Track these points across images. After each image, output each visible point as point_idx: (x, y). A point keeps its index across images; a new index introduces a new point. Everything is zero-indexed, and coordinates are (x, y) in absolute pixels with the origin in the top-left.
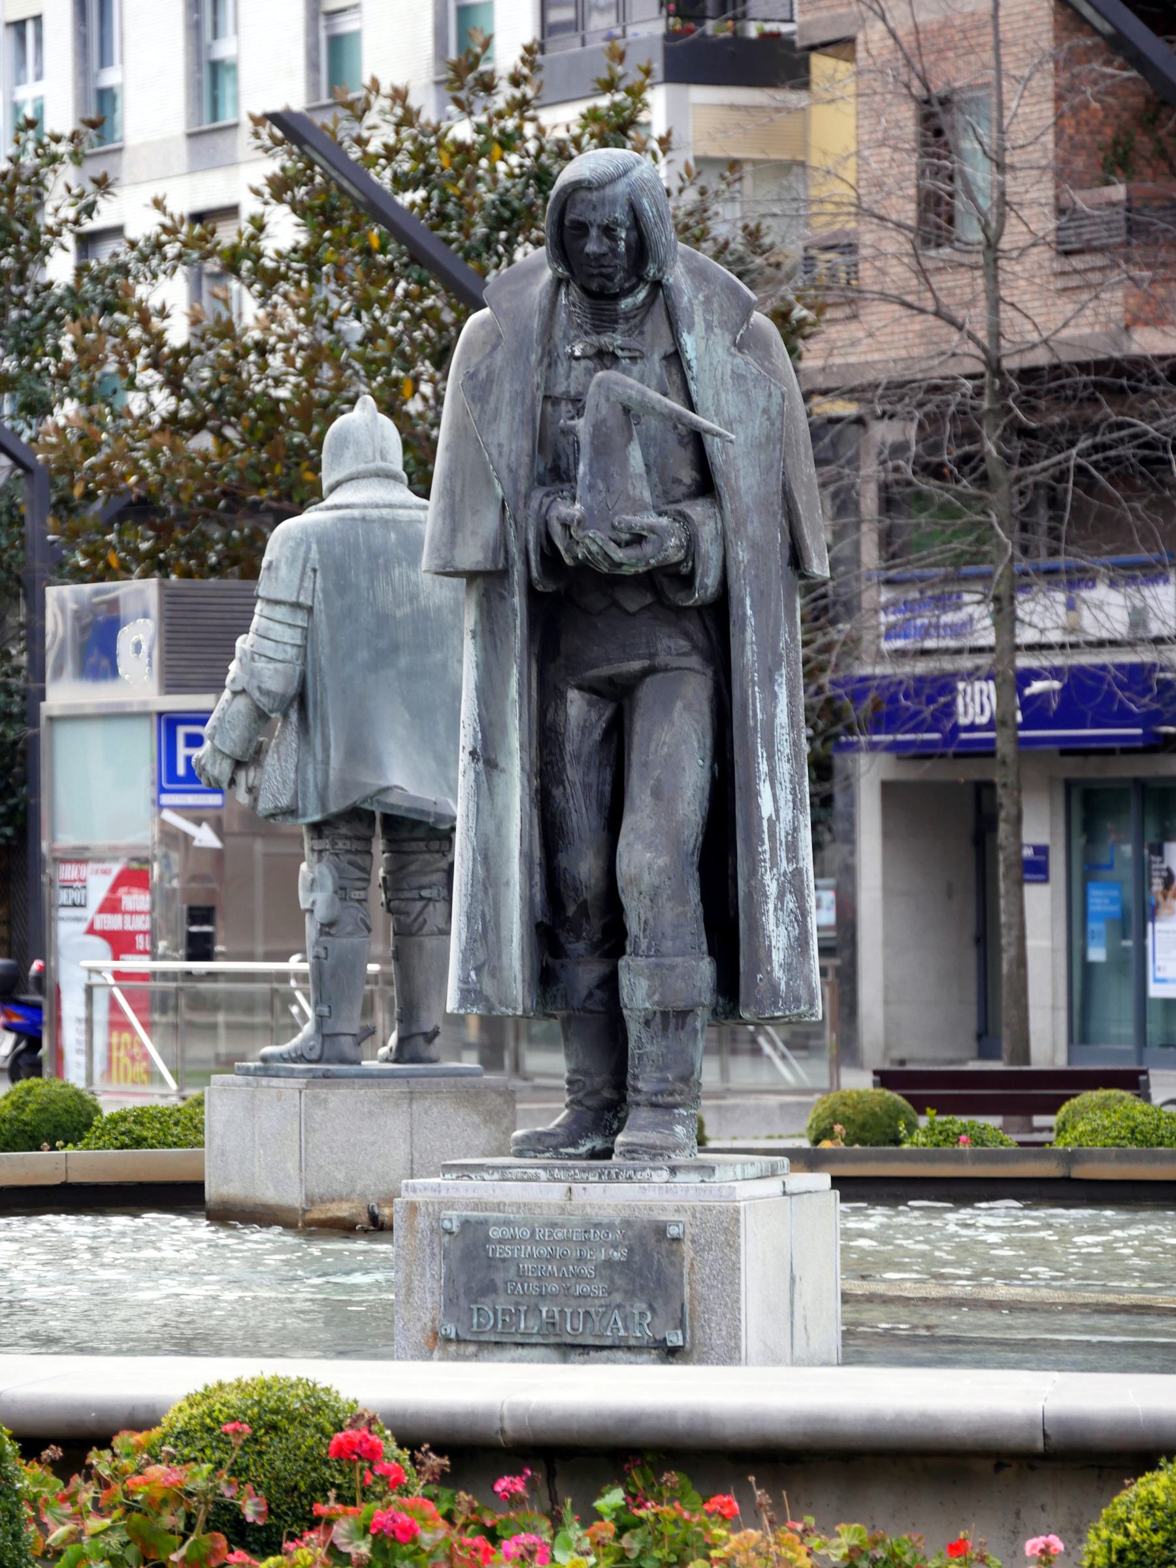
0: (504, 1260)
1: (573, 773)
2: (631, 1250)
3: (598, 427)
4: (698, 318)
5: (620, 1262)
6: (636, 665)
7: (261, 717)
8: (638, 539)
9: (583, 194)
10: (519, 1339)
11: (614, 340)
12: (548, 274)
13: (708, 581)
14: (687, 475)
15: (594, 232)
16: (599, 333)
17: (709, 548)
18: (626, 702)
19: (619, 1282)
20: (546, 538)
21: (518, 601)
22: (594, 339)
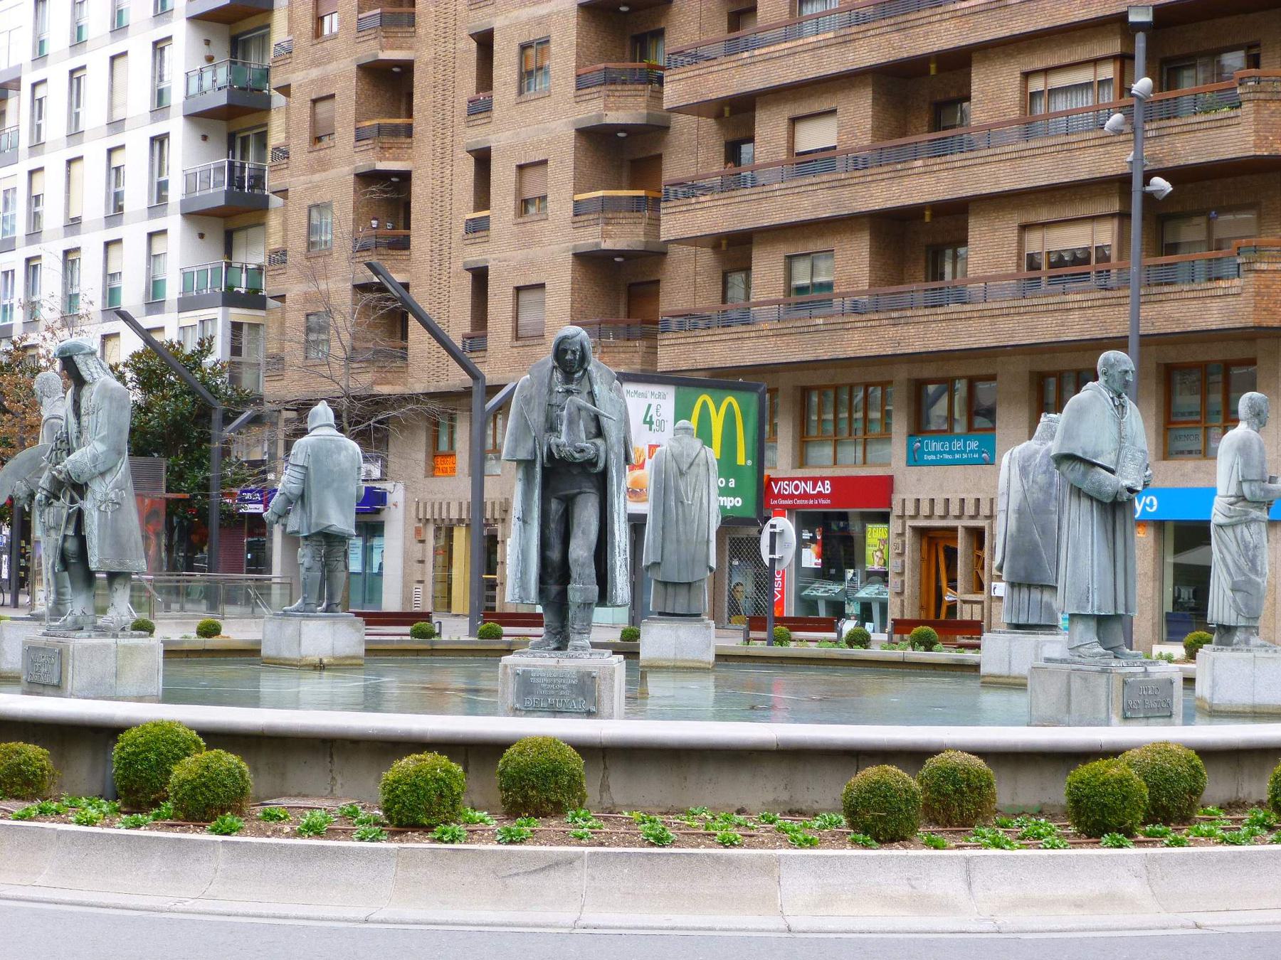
1: (553, 526)
3: (570, 414)
7: (289, 502)
8: (582, 451)
11: (573, 387)
12: (550, 364)
13: (601, 465)
14: (593, 430)
17: (602, 455)
20: (550, 449)
21: (538, 469)
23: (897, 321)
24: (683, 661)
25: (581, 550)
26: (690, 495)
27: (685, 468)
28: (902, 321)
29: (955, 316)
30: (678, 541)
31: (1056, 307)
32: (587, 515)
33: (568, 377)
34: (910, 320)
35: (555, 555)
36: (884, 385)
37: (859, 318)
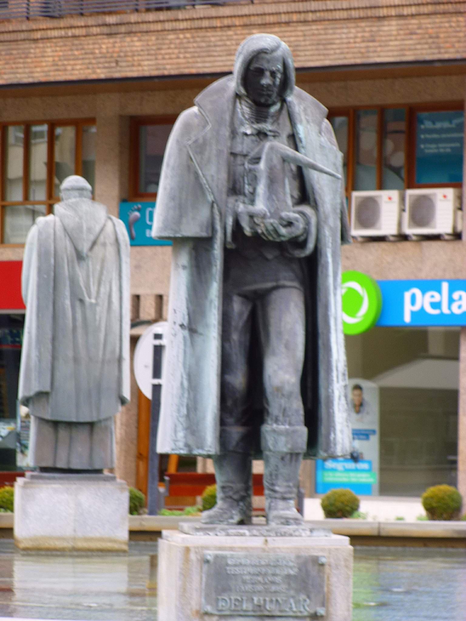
0: (234, 575)
2: (300, 569)
3: (271, 169)
4: (303, 117)
5: (295, 576)
6: (269, 285)
8: (290, 224)
9: (263, 55)
10: (242, 613)
11: (267, 126)
13: (311, 245)
15: (268, 74)
16: (258, 123)
17: (313, 230)
18: (259, 303)
19: (293, 585)
20: (237, 225)
21: (218, 251)
22: (256, 126)
23: (114, 29)
24: (87, 540)
25: (282, 371)
26: (93, 289)
27: (85, 247)
28: (123, 29)
29: (205, 23)
30: (76, 360)
31: (362, 13)
32: (288, 319)
33: (260, 110)
34: (135, 28)
35: (239, 380)
36: (81, 125)
37: (50, 24)
